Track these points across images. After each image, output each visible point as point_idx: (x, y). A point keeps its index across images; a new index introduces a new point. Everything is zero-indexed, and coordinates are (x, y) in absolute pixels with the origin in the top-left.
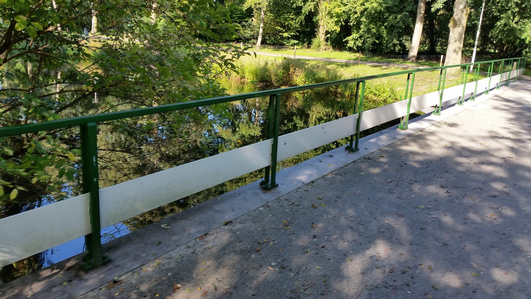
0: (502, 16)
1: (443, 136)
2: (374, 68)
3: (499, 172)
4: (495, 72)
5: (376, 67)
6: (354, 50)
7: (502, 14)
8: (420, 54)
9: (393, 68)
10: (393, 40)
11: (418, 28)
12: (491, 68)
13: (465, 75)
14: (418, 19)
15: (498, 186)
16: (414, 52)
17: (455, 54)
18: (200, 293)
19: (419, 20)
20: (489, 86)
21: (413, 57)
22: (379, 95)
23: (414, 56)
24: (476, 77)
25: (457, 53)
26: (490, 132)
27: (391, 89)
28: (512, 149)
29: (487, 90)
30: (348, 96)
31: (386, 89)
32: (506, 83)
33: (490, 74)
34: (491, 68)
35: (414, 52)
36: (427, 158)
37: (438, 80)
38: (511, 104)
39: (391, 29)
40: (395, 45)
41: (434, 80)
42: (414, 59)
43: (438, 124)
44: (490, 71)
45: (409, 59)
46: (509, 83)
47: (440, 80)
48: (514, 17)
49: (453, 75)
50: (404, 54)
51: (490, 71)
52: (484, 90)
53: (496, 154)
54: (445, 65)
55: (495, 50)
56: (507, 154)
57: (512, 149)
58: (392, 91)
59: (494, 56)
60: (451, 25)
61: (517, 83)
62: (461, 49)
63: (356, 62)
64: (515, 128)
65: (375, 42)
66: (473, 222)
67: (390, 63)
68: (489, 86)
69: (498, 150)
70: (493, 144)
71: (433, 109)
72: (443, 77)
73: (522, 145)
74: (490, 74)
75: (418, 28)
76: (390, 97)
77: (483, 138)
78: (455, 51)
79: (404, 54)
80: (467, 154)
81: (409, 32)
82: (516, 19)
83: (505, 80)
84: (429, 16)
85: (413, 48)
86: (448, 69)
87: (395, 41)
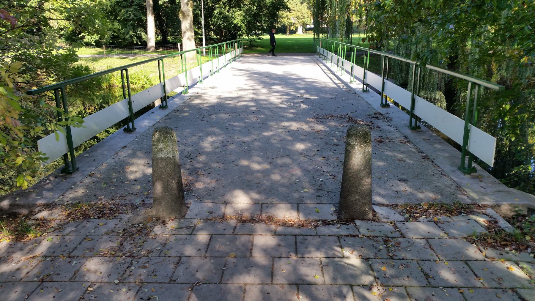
0: (216, 6)
1: (212, 94)
2: (122, 60)
3: (251, 104)
4: (221, 53)
5: (123, 58)
6: (92, 45)
7: (216, 4)
8: (158, 45)
9: (139, 58)
10: (129, 32)
11: (151, 21)
12: (216, 51)
13: (199, 59)
14: (148, 12)
15: (254, 109)
16: (152, 43)
17: (188, 41)
18: (286, 24)
19: (150, 13)
20: (219, 65)
21: (151, 47)
22: (136, 83)
23: (153, 46)
24: (211, 59)
25: (190, 40)
26: (238, 88)
27: (145, 76)
28: (253, 93)
29: (218, 69)
30: (107, 87)
31: (140, 77)
32: (234, 59)
33: (217, 56)
34: (216, 51)
35: (152, 43)
36: (210, 105)
37: (181, 65)
38: (243, 72)
39: (124, 22)
40: (131, 37)
41: (178, 65)
42: (153, 49)
43: (205, 89)
44: (217, 53)
45: (149, 49)
46: (236, 59)
47: (62, 97)
48: (225, 7)
49: (192, 59)
50: (143, 45)
51: (217, 53)
52: (223, 65)
53: (246, 97)
54: (183, 50)
55: (217, 36)
56: (252, 96)
57: (253, 93)
58: (146, 77)
59: (215, 41)
60: (180, 16)
61: (241, 59)
62: (194, 38)
63: (101, 56)
64: (252, 83)
65: (113, 35)
66: (248, 123)
67: (135, 54)
68: (219, 65)
69: (247, 95)
70: (242, 93)
71: (229, 62)
72: (184, 61)
73: (258, 91)
74: (217, 56)
75: (151, 21)
76: (146, 83)
77: (236, 91)
78: (188, 38)
79: (143, 45)
80: (231, 99)
81: (144, 26)
82: (227, 8)
83: (233, 57)
84: (156, 8)
85: (150, 39)
86: (186, 53)
87: (131, 33)
